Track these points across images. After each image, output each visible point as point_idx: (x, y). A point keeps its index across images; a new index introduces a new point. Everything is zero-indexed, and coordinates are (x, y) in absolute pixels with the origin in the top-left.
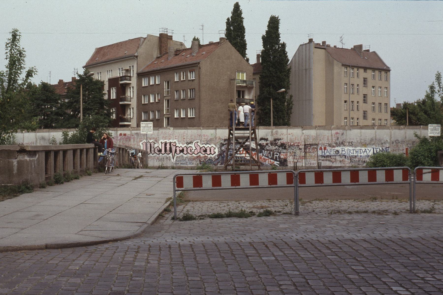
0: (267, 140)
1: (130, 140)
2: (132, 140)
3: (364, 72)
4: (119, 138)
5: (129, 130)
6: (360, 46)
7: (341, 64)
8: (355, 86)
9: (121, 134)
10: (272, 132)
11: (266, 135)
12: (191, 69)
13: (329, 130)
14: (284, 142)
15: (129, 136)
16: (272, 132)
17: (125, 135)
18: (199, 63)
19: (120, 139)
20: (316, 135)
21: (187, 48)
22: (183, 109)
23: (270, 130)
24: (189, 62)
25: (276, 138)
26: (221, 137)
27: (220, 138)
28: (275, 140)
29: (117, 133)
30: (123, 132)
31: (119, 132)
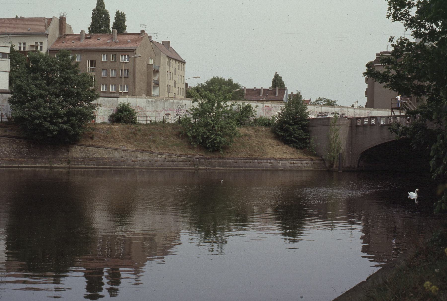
0: (338, 114)
1: (271, 110)
2: (272, 110)
3: (364, 73)
4: (265, 108)
5: (270, 104)
6: (168, 43)
7: (166, 56)
8: (171, 73)
9: (266, 106)
10: (341, 110)
11: (339, 111)
12: (123, 53)
13: (364, 110)
14: (346, 116)
15: (271, 107)
16: (341, 110)
17: (268, 107)
18: (135, 49)
19: (265, 109)
20: (359, 112)
21: (74, 34)
22: (112, 85)
23: (340, 109)
24: (128, 46)
25: (343, 113)
26: (317, 111)
27: (317, 112)
28: (343, 114)
29: (264, 105)
30: (267, 105)
31: (265, 105)
